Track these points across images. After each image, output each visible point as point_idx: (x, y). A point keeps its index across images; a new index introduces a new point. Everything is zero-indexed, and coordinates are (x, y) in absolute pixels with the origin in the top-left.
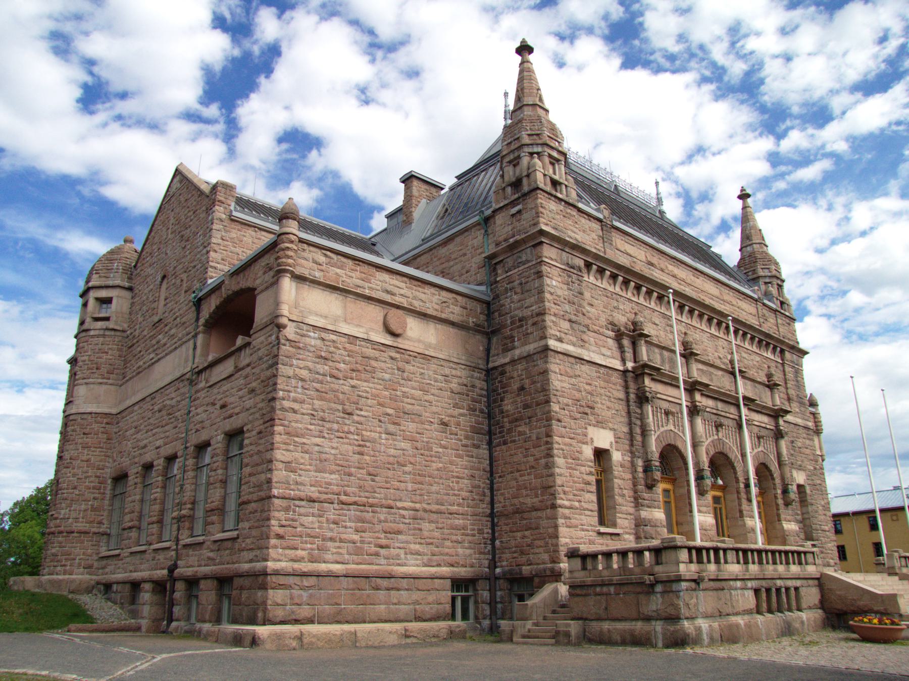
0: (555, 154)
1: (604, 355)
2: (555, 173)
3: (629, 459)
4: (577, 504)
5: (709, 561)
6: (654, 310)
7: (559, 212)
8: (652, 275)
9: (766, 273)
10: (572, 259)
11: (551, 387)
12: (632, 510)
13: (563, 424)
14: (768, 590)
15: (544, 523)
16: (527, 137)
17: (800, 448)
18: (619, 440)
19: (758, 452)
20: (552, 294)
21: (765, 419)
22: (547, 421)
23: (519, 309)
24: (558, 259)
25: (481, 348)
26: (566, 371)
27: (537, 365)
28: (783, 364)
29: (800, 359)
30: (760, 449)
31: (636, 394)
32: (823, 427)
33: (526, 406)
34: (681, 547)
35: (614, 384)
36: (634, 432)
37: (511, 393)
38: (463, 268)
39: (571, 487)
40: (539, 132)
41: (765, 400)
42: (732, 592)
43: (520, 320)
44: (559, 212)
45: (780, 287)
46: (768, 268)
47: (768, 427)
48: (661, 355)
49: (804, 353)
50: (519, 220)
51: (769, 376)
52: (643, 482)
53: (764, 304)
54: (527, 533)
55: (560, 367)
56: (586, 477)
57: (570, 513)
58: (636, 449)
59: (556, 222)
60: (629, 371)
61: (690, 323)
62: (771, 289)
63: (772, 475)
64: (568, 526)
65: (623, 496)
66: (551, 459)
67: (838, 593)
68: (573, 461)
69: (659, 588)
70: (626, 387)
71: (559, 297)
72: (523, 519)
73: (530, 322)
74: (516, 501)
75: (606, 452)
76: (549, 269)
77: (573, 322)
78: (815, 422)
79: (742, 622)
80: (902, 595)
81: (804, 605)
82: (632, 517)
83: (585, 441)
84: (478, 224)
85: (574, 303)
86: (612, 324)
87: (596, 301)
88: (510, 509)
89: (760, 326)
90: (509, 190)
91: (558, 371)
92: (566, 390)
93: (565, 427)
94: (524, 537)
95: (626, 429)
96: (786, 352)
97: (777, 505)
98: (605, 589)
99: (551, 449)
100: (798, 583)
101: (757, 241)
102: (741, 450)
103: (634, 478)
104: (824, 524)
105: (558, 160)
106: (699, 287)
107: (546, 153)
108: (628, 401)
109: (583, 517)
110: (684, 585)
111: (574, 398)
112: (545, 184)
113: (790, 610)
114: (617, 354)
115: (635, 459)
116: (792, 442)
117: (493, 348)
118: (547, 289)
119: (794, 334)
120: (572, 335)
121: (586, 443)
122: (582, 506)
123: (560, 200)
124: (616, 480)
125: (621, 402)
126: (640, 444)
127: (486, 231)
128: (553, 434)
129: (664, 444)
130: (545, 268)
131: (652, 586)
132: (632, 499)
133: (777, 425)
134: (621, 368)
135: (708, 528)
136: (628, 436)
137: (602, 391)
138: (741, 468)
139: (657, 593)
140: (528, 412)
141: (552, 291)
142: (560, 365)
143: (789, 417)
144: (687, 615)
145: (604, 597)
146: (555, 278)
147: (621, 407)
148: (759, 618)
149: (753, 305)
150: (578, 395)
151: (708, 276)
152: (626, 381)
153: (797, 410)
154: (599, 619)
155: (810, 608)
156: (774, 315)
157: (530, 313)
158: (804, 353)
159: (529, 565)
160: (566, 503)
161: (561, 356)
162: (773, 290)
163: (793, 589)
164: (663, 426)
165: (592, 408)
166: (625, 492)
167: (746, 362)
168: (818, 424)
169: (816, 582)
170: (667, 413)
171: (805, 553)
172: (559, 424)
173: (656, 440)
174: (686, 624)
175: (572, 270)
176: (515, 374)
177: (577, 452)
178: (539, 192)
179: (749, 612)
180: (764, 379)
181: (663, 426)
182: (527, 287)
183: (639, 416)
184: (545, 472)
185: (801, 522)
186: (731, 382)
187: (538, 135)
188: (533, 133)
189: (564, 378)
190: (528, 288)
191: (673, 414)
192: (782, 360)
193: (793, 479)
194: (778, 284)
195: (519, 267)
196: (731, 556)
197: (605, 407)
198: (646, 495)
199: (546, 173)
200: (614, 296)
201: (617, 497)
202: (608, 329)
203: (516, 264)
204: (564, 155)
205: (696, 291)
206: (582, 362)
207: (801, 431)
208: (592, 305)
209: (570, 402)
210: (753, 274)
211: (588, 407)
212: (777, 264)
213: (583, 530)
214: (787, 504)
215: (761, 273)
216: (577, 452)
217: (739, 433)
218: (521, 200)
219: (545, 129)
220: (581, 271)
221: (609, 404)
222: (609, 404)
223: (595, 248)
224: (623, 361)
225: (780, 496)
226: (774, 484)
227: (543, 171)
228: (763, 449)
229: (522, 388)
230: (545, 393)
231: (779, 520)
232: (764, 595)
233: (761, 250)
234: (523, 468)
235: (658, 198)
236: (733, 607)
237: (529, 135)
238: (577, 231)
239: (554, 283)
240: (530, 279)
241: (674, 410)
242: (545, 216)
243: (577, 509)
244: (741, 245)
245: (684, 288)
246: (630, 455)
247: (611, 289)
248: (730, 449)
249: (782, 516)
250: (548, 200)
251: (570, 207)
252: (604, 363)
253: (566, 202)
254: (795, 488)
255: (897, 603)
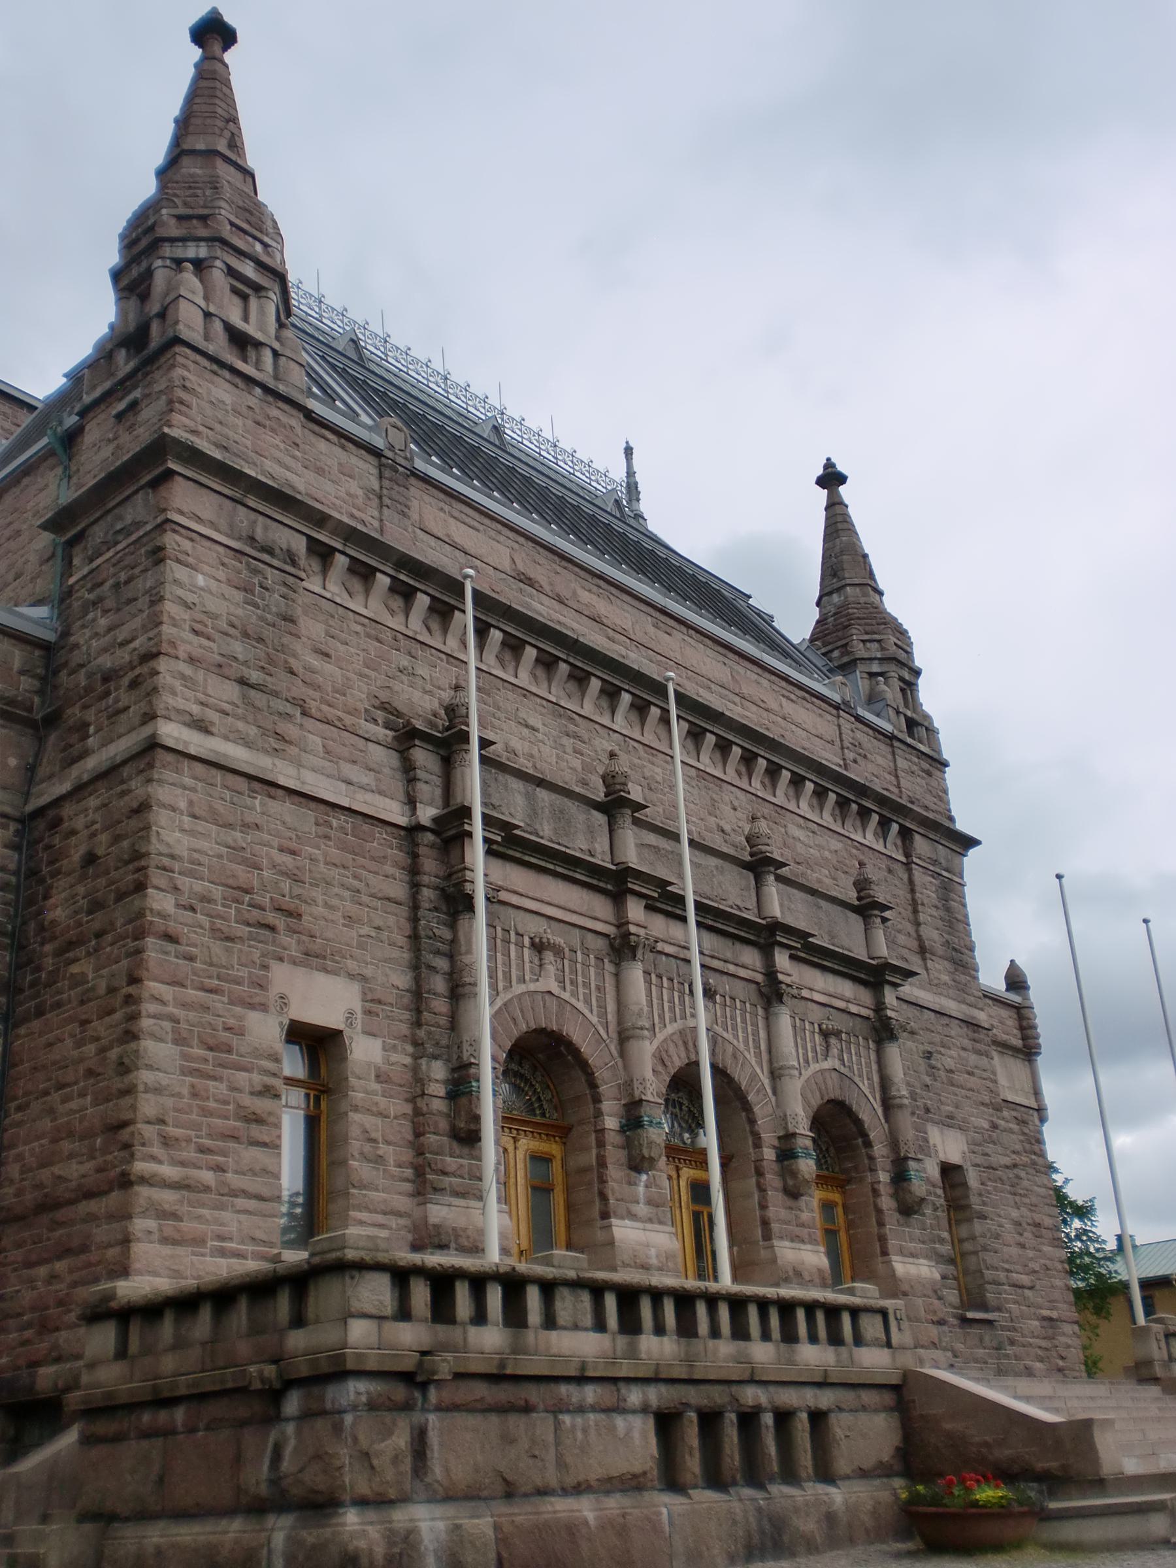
0: (248, 270)
1: (349, 783)
2: (246, 319)
3: (408, 1060)
4: (208, 1177)
5: (480, 1317)
6: (526, 693)
7: (244, 410)
8: (529, 608)
9: (874, 651)
10: (266, 528)
11: (155, 846)
12: (402, 1202)
13: (181, 948)
14: (710, 1420)
15: (101, 1233)
16: (173, 221)
17: (951, 1071)
18: (375, 1007)
19: (822, 1071)
20: (188, 606)
21: (846, 988)
22: (136, 939)
23: (105, 650)
24: (223, 524)
25: (13, 762)
26: (213, 811)
27: (130, 791)
28: (908, 865)
29: (956, 858)
30: (826, 1065)
31: (443, 890)
32: (1041, 1041)
33: (96, 906)
34: (362, 1266)
35: (373, 858)
36: (426, 987)
37: (69, 874)
38: (11, 566)
39: (196, 1127)
40: (206, 212)
41: (846, 942)
42: (567, 1419)
43: (106, 679)
44: (244, 410)
45: (909, 687)
46: (879, 641)
47: (854, 1009)
48: (530, 798)
49: (969, 842)
50: (131, 428)
51: (862, 885)
52: (443, 1125)
53: (859, 719)
54: (60, 1266)
55: (194, 796)
56: (247, 1101)
57: (181, 1202)
58: (429, 1033)
59: (226, 431)
60: (423, 828)
61: (637, 736)
62: (883, 687)
63: (864, 1135)
64: (165, 1240)
65: (379, 1160)
66: (133, 1045)
67: (948, 1426)
68: (210, 1055)
69: (292, 1404)
70: (414, 870)
71: (215, 617)
72: (57, 1224)
73: (126, 681)
74: (45, 1175)
75: (333, 1036)
76: (187, 545)
77: (252, 686)
78: (1022, 1028)
79: (590, 1516)
80: (1108, 1423)
81: (842, 1465)
82: (403, 1221)
83: (256, 1000)
84: (47, 455)
85: (261, 640)
86: (385, 707)
87: (342, 648)
88: (30, 1198)
89: (846, 767)
90: (122, 355)
91: (183, 805)
92: (204, 859)
93: (191, 958)
94: (53, 1278)
95: (402, 980)
96: (917, 837)
97: (879, 1211)
98: (163, 1416)
99: (134, 1017)
100: (825, 1399)
101: (857, 581)
102: (770, 1062)
103: (417, 1112)
104: (1019, 1268)
105: (258, 288)
106: (671, 655)
107: (218, 263)
108: (415, 907)
109: (226, 1215)
110: (356, 1390)
111: (231, 882)
112: (207, 337)
113: (790, 1475)
114: (397, 786)
115: (423, 1061)
116: (928, 1055)
117: (45, 760)
118: (169, 590)
119: (941, 799)
120: (244, 719)
121: (263, 1007)
122: (224, 1183)
123: (250, 380)
124: (355, 1117)
125: (393, 907)
126: (443, 1021)
127: (66, 468)
128: (144, 974)
129: (524, 1028)
130: (170, 540)
131: (275, 1395)
132: (409, 1173)
133: (879, 1007)
134: (402, 821)
135: (654, 1261)
136: (407, 999)
137: (335, 873)
138: (769, 1109)
139: (287, 1420)
140: (98, 921)
141: (190, 598)
142: (193, 790)
143: (908, 989)
144: (364, 1488)
145: (159, 1442)
146: (206, 568)
147: (395, 922)
148: (666, 1505)
149: (829, 717)
150: (243, 875)
151: (698, 631)
152: (415, 856)
153: (945, 978)
154: (143, 1516)
155: (863, 1474)
156: (889, 749)
157: (127, 658)
158: (969, 842)
159: (58, 1360)
160: (168, 1171)
161: (199, 768)
162: (891, 692)
163: (804, 1416)
164: (522, 980)
165: (296, 915)
166: (383, 1149)
167: (800, 848)
168: (1029, 1032)
169: (888, 1398)
170: (539, 947)
171: (855, 1312)
172: (171, 947)
173: (495, 1016)
174: (351, 1518)
175: (266, 557)
176: (80, 823)
177: (228, 1029)
178: (178, 349)
179: (632, 1484)
180: (851, 895)
181: (522, 980)
182: (127, 593)
183: (444, 948)
184: (118, 1084)
185: (952, 1261)
186: (748, 889)
187: (204, 219)
188: (190, 212)
189: (201, 826)
190: (130, 595)
191: (558, 951)
192: (907, 855)
193: (925, 1147)
194: (901, 679)
195: (116, 543)
196: (569, 1305)
197: (338, 916)
198: (451, 1163)
199: (212, 309)
200: (403, 642)
201: (353, 1163)
202: (375, 721)
203: (109, 537)
204: (280, 277)
205: (659, 663)
206: (272, 791)
207: (956, 1030)
208: (327, 655)
209: (217, 892)
210: (842, 655)
211: (279, 909)
212: (901, 633)
213: (222, 1252)
214: (908, 1209)
215: (860, 650)
216: (228, 1029)
217: (767, 1018)
218: (140, 375)
219: (223, 204)
220: (294, 563)
221: (353, 909)
222: (353, 909)
223: (352, 516)
224: (411, 802)
225: (885, 1189)
226: (871, 1158)
227: (203, 304)
228: (837, 1065)
229: (90, 859)
230: (136, 864)
231: (885, 1253)
232: (691, 1434)
233: (862, 600)
234: (70, 1078)
235: (628, 484)
236: (561, 1464)
237: (180, 218)
238: (298, 466)
239: (201, 580)
240: (137, 571)
241: (559, 940)
242: (194, 412)
243: (207, 1189)
244: (821, 590)
245: (623, 651)
246: (410, 1049)
247: (396, 623)
248: (734, 1056)
249: (893, 1243)
250: (208, 375)
251: (281, 404)
252: (345, 802)
253: (267, 390)
254: (934, 1172)
255: (1092, 1447)
